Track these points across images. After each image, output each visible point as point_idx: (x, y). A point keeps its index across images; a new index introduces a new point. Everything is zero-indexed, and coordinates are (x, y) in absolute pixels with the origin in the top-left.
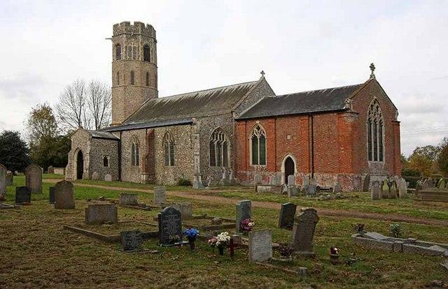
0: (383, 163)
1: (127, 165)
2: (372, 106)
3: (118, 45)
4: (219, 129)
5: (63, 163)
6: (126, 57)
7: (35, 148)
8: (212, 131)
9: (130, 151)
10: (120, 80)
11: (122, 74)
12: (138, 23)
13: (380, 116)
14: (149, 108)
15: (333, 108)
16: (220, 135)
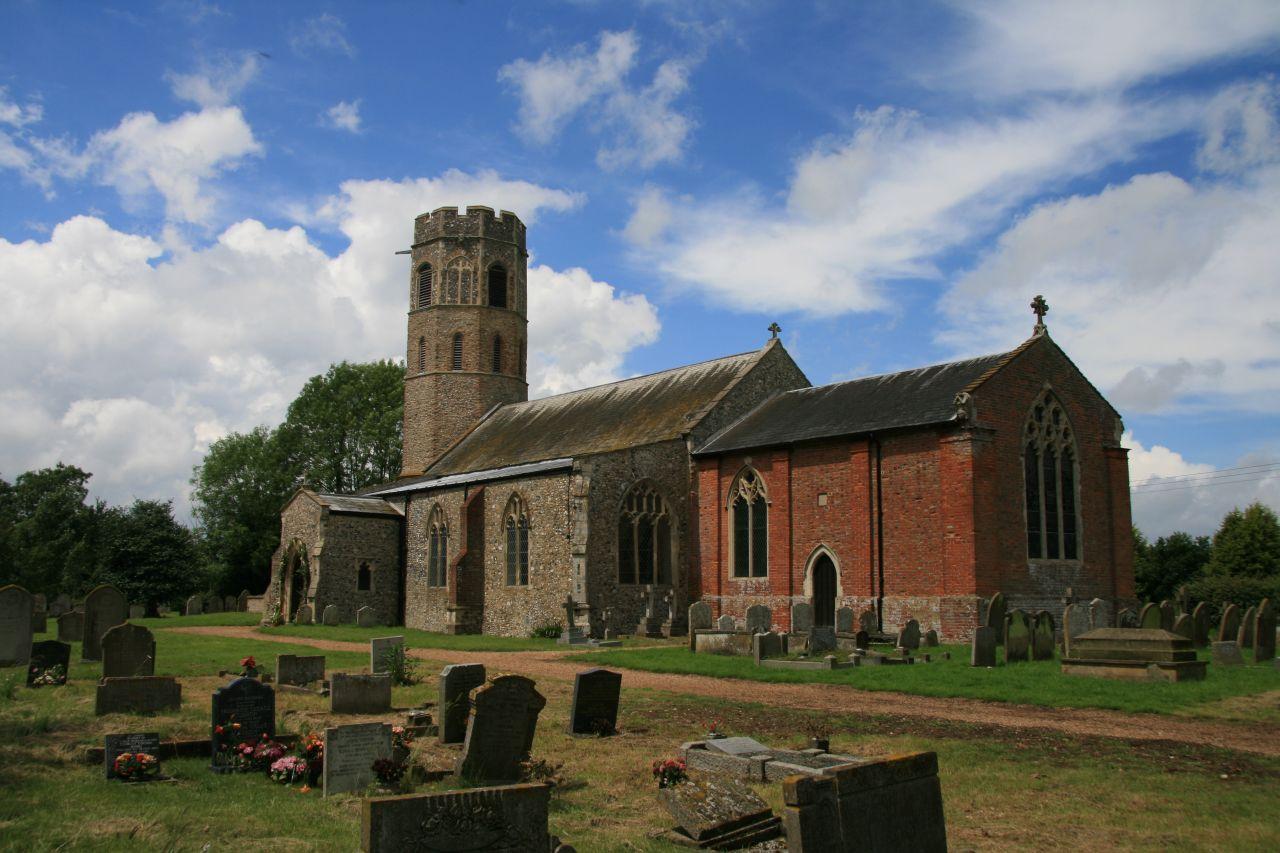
1: (417, 584)
2: (1039, 410)
6: (443, 297)
9: (427, 547)
11: (431, 343)
13: (1066, 435)
16: (650, 497)
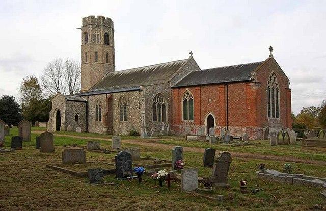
0: (279, 119)
1: (92, 120)
2: (271, 77)
3: (86, 33)
4: (159, 94)
5: (46, 119)
6: (91, 42)
7: (26, 108)
8: (154, 95)
9: (95, 110)
10: (87, 59)
11: (89, 54)
12: (101, 17)
13: (277, 85)
14: (108, 79)
15: (242, 79)
16: (160, 98)
